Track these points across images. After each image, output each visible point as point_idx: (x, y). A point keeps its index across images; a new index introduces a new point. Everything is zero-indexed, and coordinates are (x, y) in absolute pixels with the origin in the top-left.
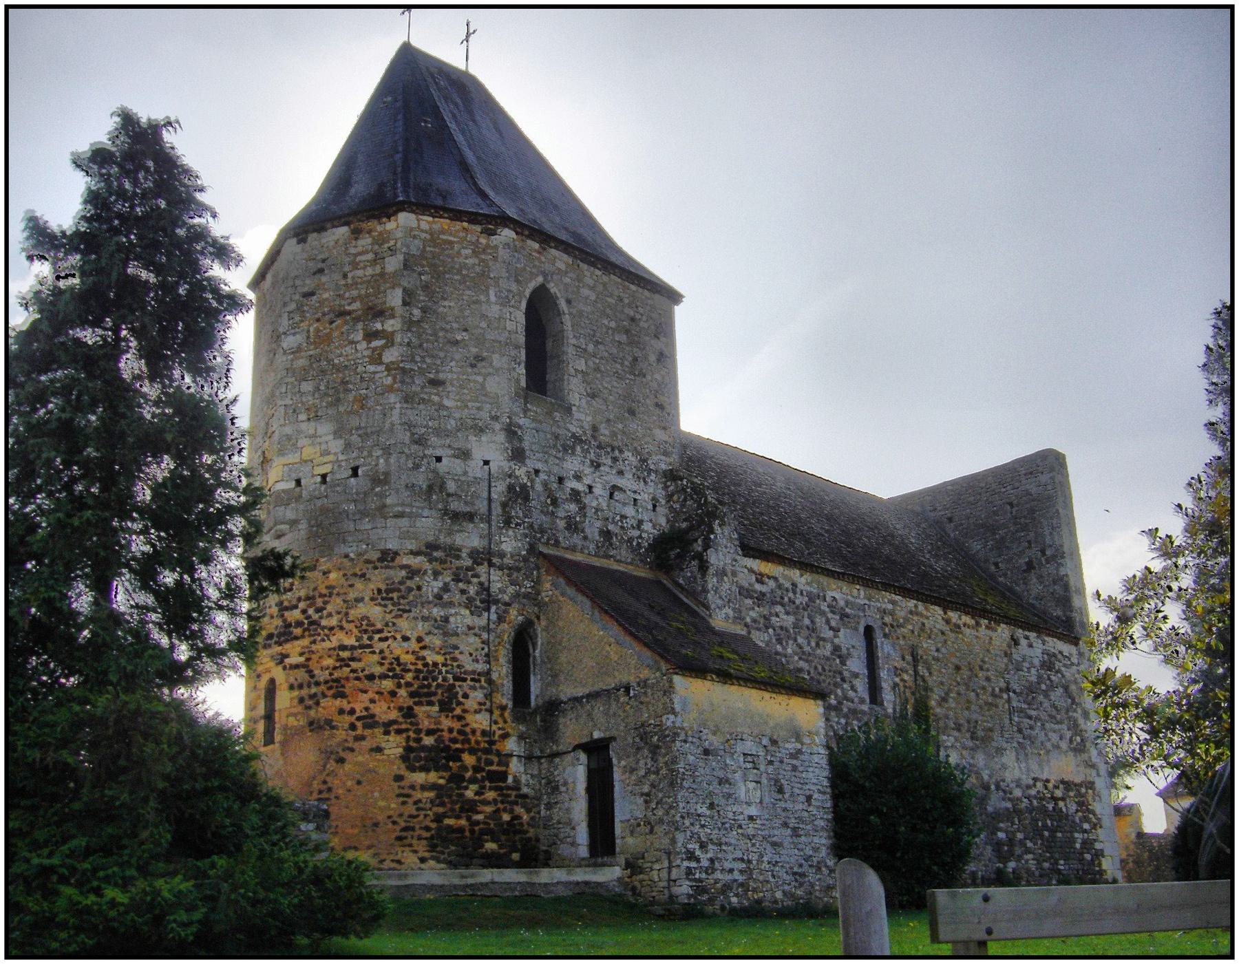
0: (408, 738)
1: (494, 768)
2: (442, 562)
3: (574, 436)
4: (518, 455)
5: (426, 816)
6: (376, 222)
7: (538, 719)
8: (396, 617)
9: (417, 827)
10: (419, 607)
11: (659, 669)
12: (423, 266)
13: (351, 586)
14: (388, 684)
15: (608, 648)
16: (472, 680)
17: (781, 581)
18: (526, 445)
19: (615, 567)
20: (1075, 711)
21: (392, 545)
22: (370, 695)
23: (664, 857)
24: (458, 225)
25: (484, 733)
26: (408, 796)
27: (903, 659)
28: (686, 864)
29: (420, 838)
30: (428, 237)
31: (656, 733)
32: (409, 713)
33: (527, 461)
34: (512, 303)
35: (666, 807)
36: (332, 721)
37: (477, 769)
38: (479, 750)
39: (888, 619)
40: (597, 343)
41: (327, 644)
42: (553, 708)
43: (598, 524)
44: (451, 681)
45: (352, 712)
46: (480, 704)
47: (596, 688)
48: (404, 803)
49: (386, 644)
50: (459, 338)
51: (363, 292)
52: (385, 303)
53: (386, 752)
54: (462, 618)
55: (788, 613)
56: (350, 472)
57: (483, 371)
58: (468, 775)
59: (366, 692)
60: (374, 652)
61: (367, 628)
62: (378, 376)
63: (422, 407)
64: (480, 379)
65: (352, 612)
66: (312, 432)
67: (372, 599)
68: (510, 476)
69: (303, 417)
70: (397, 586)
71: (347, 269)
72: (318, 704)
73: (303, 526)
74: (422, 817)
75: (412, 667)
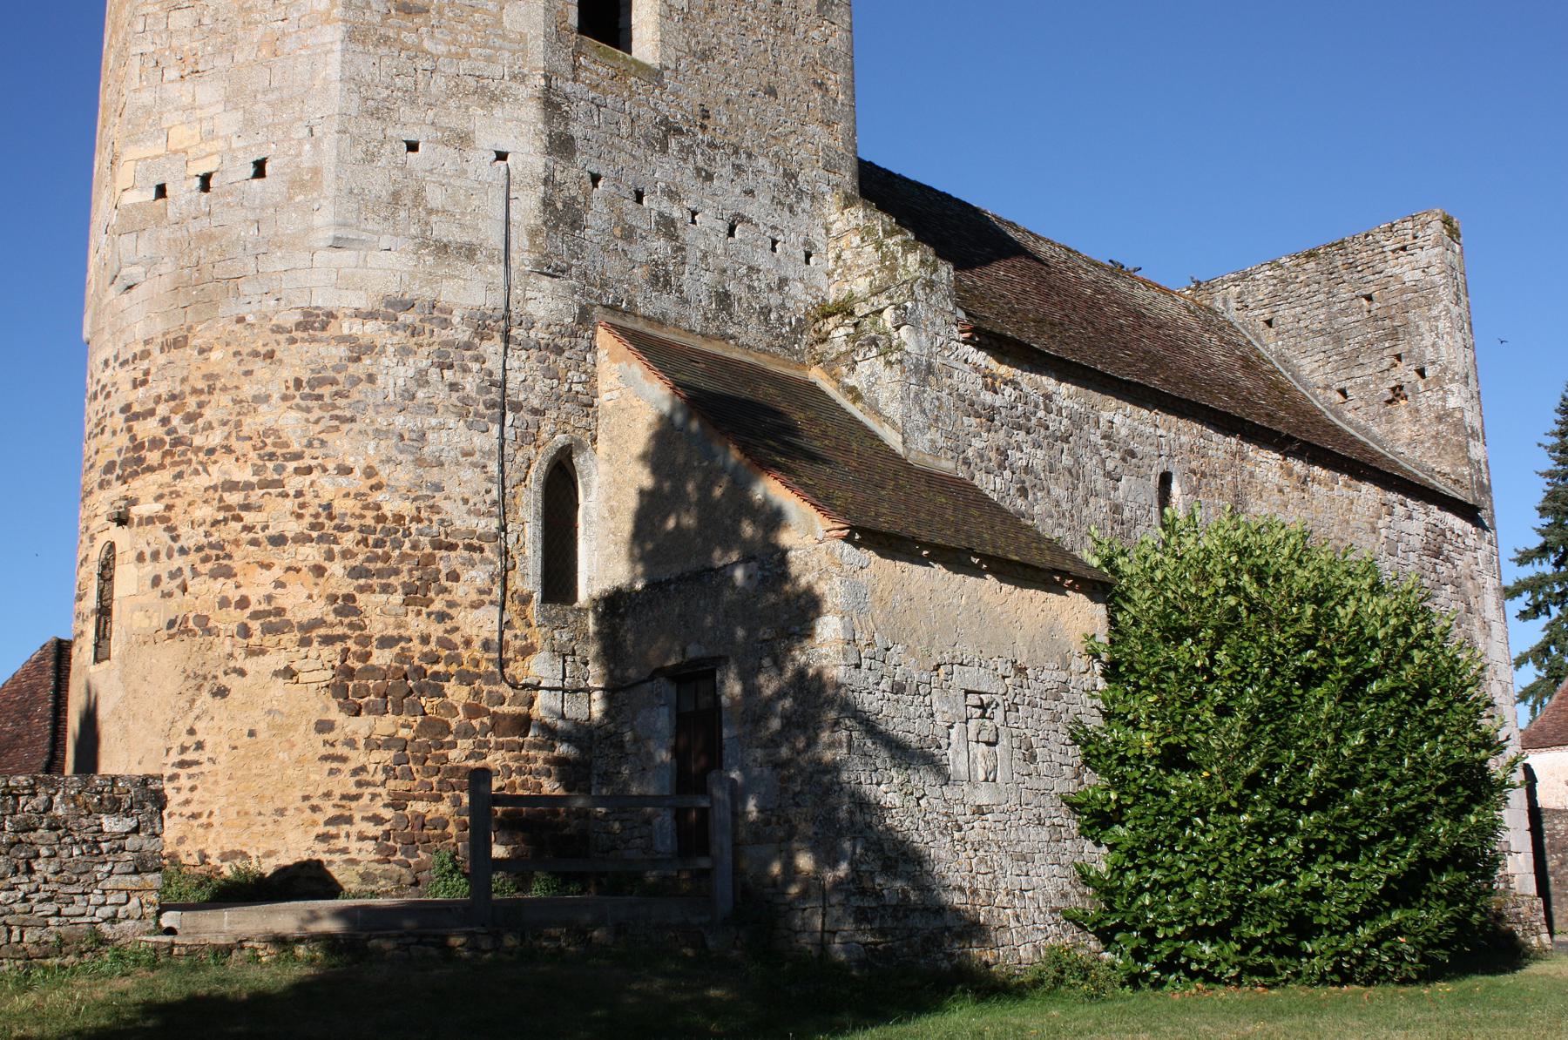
3: (665, 121)
4: (561, 146)
5: (374, 796)
8: (328, 430)
9: (357, 817)
10: (371, 412)
13: (248, 373)
14: (311, 553)
16: (470, 548)
18: (576, 130)
22: (277, 572)
26: (343, 759)
32: (346, 606)
36: (207, 618)
37: (473, 711)
38: (479, 676)
41: (203, 481)
44: (428, 550)
45: (243, 603)
46: (481, 592)
49: (308, 479)
53: (302, 677)
59: (268, 567)
61: (272, 450)
63: (383, 50)
65: (247, 421)
66: (186, 100)
67: (285, 398)
69: (172, 74)
70: (330, 374)
73: (167, 267)
74: (366, 799)
75: (355, 523)
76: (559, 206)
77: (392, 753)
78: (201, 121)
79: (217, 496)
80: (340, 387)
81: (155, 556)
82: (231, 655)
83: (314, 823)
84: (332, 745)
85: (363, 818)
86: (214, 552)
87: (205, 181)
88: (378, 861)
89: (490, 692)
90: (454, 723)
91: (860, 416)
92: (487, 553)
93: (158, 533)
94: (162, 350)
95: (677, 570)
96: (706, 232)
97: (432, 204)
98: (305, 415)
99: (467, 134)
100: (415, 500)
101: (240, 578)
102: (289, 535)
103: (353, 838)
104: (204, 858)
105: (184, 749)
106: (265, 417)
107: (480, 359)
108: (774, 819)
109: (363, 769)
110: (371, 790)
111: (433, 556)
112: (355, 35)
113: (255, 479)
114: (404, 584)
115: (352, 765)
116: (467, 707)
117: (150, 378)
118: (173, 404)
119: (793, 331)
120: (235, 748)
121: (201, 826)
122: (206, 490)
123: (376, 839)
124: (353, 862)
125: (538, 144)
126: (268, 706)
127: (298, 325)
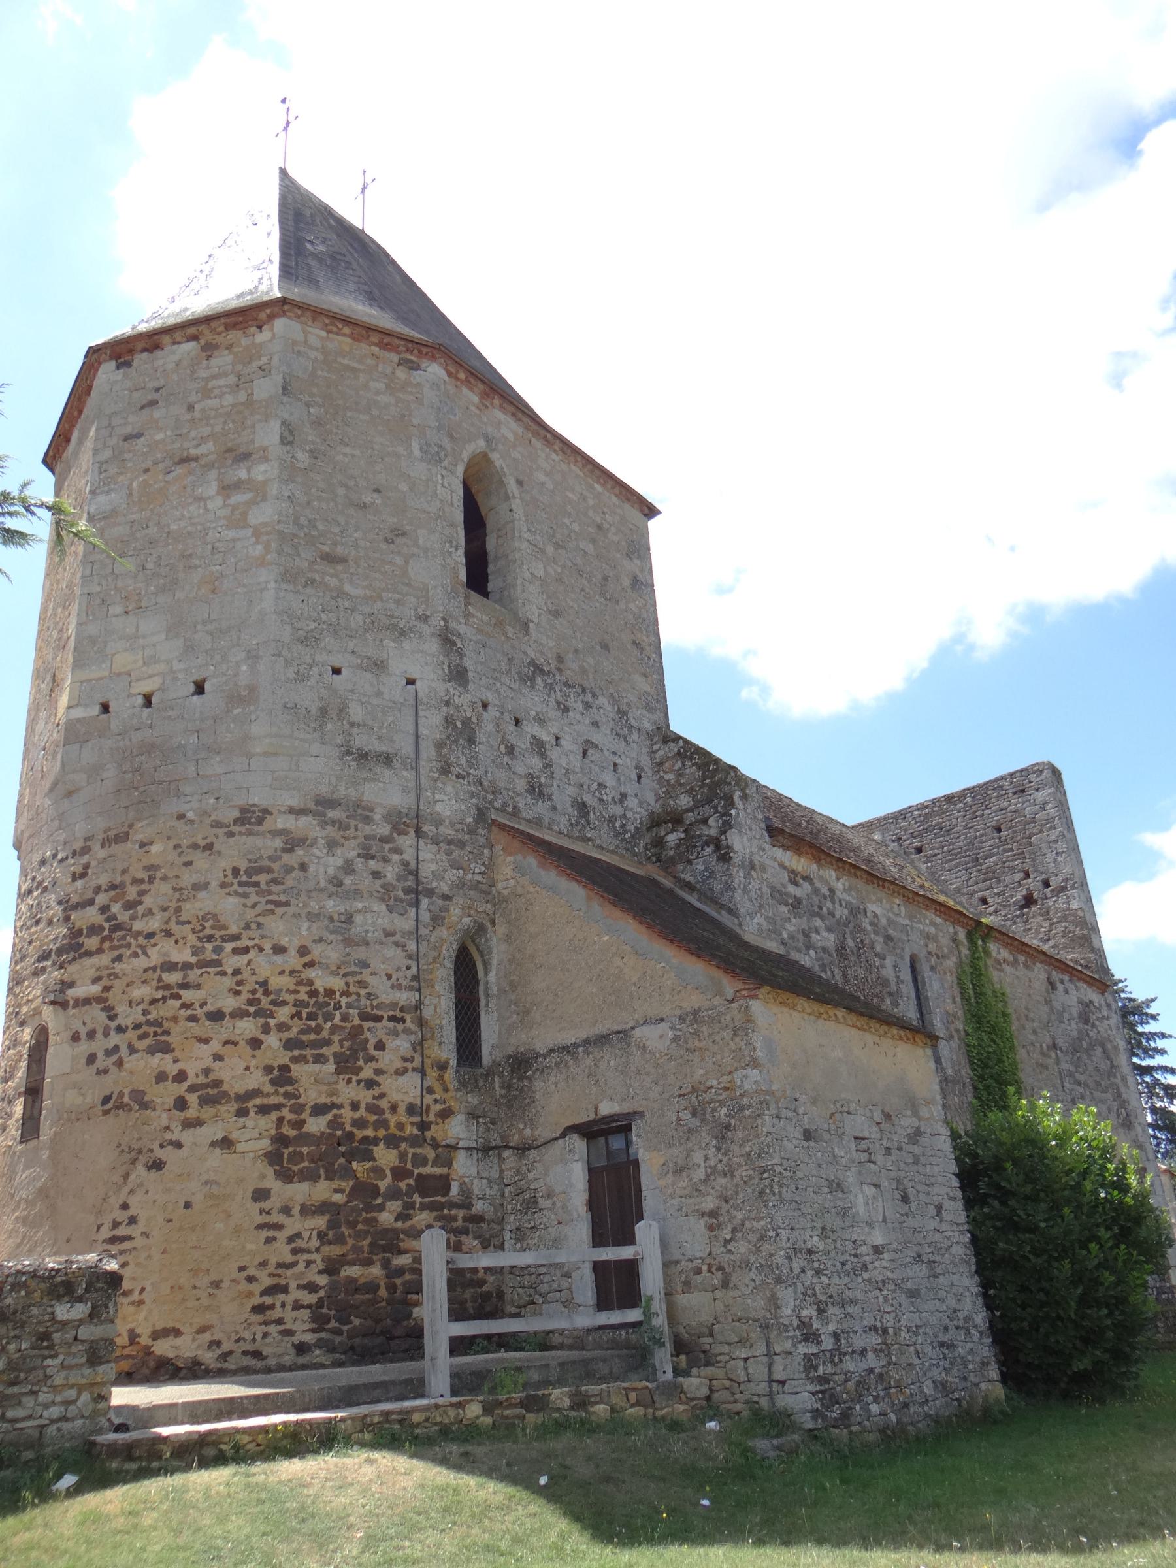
0: (280, 1120)
1: (428, 1170)
2: (342, 826)
3: (532, 663)
4: (459, 675)
5: (309, 1263)
6: (239, 333)
7: (497, 1085)
8: (264, 913)
9: (293, 1285)
10: (303, 897)
11: (720, 992)
12: (312, 395)
13: (188, 864)
14: (247, 1027)
15: (618, 962)
16: (392, 1019)
17: (818, 884)
18: (468, 663)
19: (596, 854)
20: (1115, 1076)
21: (259, 798)
22: (215, 1046)
23: (756, 1334)
24: (364, 348)
25: (411, 1109)
26: (278, 1227)
27: (954, 1002)
28: (803, 1349)
29: (297, 1306)
30: (320, 357)
31: (722, 1103)
32: (282, 1077)
33: (471, 686)
34: (445, 463)
35: (753, 1238)
36: (143, 1093)
37: (399, 1173)
38: (403, 1139)
39: (932, 947)
40: (557, 546)
41: (142, 962)
42: (521, 1064)
43: (571, 790)
44: (357, 1021)
45: (181, 1077)
46: (405, 1060)
47: (601, 1029)
48: (269, 1241)
49: (245, 958)
50: (368, 500)
51: (218, 429)
52: (253, 441)
53: (240, 1147)
54: (374, 918)
55: (829, 930)
56: (192, 688)
57: (405, 550)
58: (383, 1185)
59: (206, 1041)
60: (224, 974)
61: (211, 932)
62: (239, 545)
63: (309, 590)
64: (399, 560)
65: (187, 906)
66: (130, 630)
67: (223, 885)
68: (447, 704)
69: (118, 609)
70: (267, 863)
71: (193, 398)
72: (120, 1064)
73: (110, 772)
74: (301, 1266)
75: (290, 998)
76: (459, 724)
77: (327, 1217)
78: (143, 647)
79: (156, 976)
80: (275, 875)
81: (91, 1035)
82: (168, 1128)
83: (250, 1294)
84: (268, 1213)
85: (299, 1287)
86: (152, 1029)
87: (148, 701)
88: (313, 1331)
89: (414, 1155)
90: (383, 1185)
91: (698, 905)
92: (408, 1024)
93: (96, 1016)
94: (103, 846)
95: (583, 1035)
96: (566, 757)
97: (354, 719)
98: (243, 900)
99: (382, 662)
100: (344, 975)
101: (177, 1053)
102: (227, 1010)
103: (289, 1307)
104: (133, 1337)
105: (116, 1225)
106: (203, 903)
107: (398, 851)
108: (705, 1268)
109: (298, 1235)
110: (306, 1257)
111: (361, 1027)
112: (287, 576)
113: (193, 960)
114: (335, 1055)
115: (288, 1232)
116: (394, 1170)
117: (90, 871)
118: (113, 893)
119: (633, 836)
120: (171, 1221)
121: (133, 1303)
122: (145, 971)
123: (309, 1306)
124: (289, 1333)
125: (440, 672)
126: (205, 1177)
127: (236, 821)
